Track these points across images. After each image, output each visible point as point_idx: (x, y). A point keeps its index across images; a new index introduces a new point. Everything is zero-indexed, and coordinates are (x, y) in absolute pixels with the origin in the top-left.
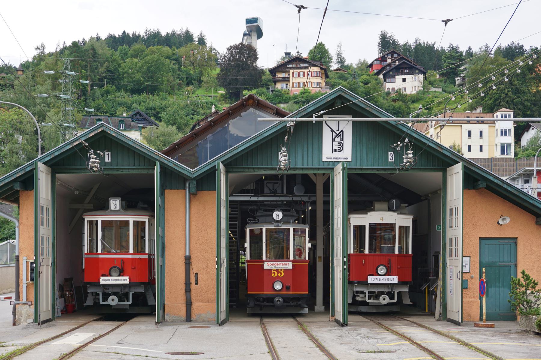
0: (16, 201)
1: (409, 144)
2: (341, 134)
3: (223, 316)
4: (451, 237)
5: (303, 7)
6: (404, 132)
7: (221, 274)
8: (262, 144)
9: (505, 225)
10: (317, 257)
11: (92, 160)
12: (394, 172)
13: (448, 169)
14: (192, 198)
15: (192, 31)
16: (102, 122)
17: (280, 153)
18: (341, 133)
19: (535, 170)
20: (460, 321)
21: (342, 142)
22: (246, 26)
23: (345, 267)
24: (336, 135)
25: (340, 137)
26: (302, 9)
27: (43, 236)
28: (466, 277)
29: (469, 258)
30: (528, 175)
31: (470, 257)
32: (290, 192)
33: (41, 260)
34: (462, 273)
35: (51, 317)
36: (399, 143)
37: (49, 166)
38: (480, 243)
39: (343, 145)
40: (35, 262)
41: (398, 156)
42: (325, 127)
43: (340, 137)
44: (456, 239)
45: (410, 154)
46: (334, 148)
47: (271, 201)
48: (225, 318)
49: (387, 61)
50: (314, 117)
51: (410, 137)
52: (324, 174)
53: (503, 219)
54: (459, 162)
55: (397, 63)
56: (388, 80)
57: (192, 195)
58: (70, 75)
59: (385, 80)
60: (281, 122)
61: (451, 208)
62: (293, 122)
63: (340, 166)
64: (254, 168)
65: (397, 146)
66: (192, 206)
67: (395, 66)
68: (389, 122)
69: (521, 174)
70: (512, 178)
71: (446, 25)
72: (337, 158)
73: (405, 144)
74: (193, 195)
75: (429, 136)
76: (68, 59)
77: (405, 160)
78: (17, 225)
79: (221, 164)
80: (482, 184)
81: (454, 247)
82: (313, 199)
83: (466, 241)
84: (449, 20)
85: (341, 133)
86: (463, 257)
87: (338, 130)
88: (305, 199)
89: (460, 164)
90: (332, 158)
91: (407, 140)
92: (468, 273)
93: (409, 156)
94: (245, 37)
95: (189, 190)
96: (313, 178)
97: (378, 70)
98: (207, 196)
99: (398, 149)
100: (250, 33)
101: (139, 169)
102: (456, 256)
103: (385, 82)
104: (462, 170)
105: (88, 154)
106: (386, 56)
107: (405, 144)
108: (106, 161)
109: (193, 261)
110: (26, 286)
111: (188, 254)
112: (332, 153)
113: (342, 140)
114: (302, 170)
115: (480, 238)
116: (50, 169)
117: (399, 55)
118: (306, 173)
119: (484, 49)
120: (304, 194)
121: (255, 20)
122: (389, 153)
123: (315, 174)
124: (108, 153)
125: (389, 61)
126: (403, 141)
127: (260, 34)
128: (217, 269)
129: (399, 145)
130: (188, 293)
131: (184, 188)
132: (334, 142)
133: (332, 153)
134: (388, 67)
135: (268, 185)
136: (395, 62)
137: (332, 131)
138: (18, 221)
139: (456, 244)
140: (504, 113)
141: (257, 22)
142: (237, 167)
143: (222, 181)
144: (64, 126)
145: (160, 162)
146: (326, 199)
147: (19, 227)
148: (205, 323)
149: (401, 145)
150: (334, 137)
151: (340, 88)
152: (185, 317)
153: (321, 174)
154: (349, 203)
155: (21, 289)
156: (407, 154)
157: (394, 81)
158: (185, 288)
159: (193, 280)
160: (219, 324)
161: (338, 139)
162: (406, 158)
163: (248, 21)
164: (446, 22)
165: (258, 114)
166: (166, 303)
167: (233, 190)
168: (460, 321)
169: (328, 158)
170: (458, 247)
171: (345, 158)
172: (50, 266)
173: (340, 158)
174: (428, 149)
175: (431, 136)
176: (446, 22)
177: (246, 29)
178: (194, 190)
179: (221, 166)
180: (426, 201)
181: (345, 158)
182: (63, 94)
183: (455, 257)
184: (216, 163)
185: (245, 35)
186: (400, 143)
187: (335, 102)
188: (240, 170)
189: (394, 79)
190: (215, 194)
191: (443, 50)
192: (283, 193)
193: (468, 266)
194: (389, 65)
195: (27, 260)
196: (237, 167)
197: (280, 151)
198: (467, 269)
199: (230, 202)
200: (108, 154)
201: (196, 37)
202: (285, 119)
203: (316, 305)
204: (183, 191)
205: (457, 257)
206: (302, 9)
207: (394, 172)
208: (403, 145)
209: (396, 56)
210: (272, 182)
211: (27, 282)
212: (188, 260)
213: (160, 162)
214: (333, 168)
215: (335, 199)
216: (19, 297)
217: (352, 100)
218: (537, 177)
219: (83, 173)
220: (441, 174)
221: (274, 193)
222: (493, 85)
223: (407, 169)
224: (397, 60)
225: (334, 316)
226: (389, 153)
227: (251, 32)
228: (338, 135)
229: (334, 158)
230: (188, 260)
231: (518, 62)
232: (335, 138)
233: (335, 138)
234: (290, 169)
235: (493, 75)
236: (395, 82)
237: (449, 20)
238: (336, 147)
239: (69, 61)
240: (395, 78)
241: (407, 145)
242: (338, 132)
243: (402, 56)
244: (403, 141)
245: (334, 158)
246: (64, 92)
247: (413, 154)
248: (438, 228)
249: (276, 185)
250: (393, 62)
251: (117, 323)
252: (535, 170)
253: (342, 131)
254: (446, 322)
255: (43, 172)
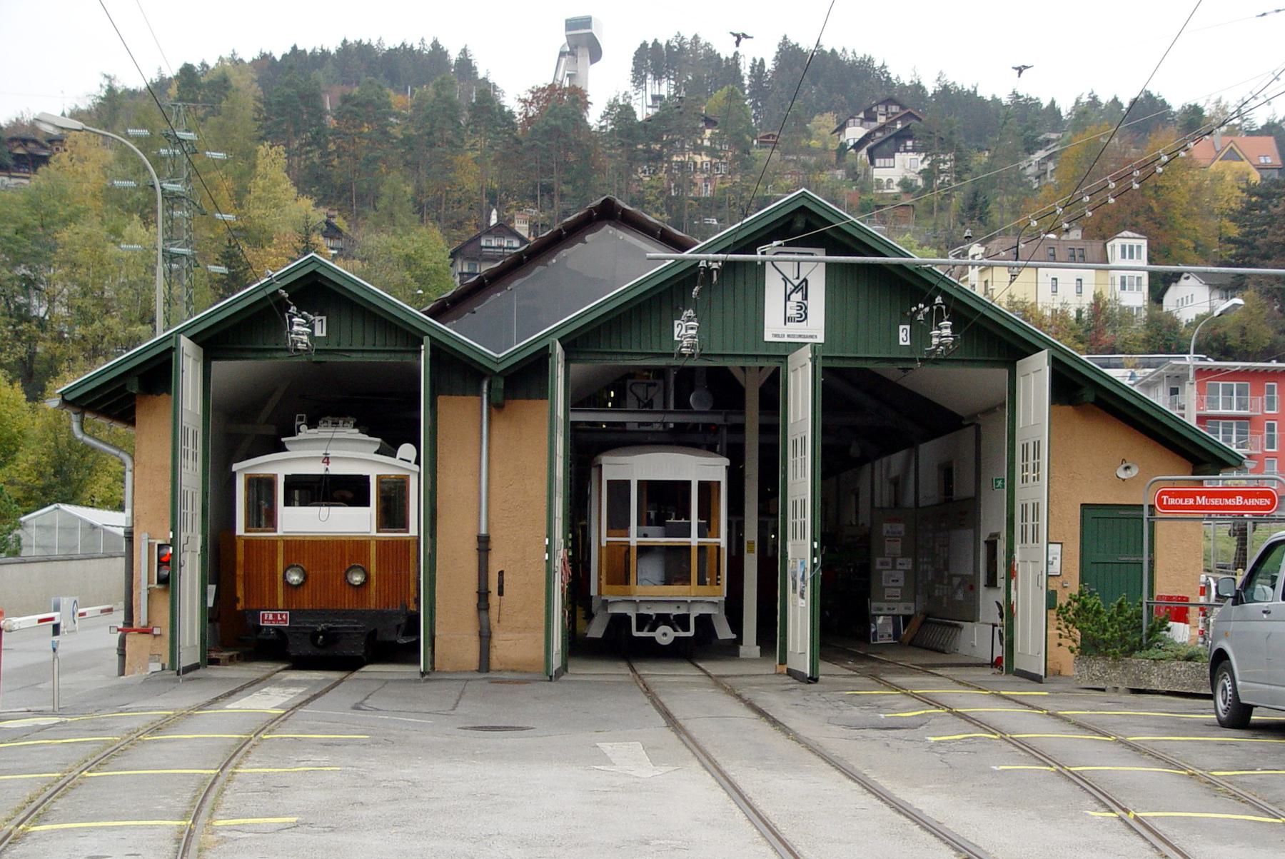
0: (128, 418)
1: (944, 307)
2: (803, 287)
3: (556, 662)
4: (1024, 503)
5: (744, 36)
6: (931, 285)
7: (555, 572)
8: (640, 304)
9: (1132, 479)
10: (746, 544)
11: (295, 328)
12: (910, 366)
13: (1019, 363)
14: (494, 418)
15: (445, 44)
16: (313, 254)
17: (676, 322)
18: (804, 284)
19: (1191, 367)
20: (1043, 673)
21: (805, 302)
22: (567, 36)
23: (815, 560)
24: (793, 288)
25: (800, 293)
26: (743, 40)
27: (187, 489)
28: (1054, 585)
29: (1060, 546)
30: (1177, 377)
31: (1061, 543)
32: (682, 405)
33: (183, 540)
34: (1048, 576)
35: (198, 660)
36: (921, 306)
37: (198, 344)
38: (1082, 516)
39: (806, 308)
40: (173, 542)
41: (920, 334)
42: (770, 272)
43: (800, 293)
44: (1036, 507)
45: (946, 328)
46: (788, 315)
47: (640, 424)
48: (560, 665)
49: (875, 120)
50: (759, 253)
51: (946, 295)
52: (761, 368)
53: (1127, 468)
54: (1041, 350)
55: (899, 126)
56: (878, 162)
57: (493, 409)
58: (184, 140)
59: (872, 163)
60: (679, 262)
61: (1025, 442)
62: (717, 262)
63: (806, 353)
64: (623, 354)
65: (918, 311)
66: (495, 432)
67: (895, 131)
68: (907, 266)
69: (1163, 374)
70: (1144, 384)
71: (1019, 76)
72: (793, 336)
73: (935, 307)
74: (496, 406)
75: (967, 287)
76: (180, 104)
77: (935, 341)
78: (129, 465)
79: (558, 343)
80: (1089, 396)
81: (1030, 523)
82: (735, 419)
83: (1054, 509)
84: (1026, 67)
85: (804, 284)
86: (1048, 543)
87: (798, 278)
88: (717, 419)
89: (1045, 352)
90: (784, 336)
91: (938, 300)
92: (1058, 576)
93: (944, 332)
94: (563, 60)
95: (489, 397)
96: (739, 375)
97: (856, 141)
98: (529, 412)
99: (919, 318)
100: (575, 50)
101: (384, 351)
102: (1036, 538)
103: (872, 167)
104: (1048, 364)
105: (287, 315)
106: (875, 109)
107: (935, 307)
108: (766, 339)
109: (494, 545)
110: (148, 595)
111: (483, 531)
112: (785, 324)
113: (805, 297)
114: (722, 359)
115: (1082, 505)
116: (201, 350)
117: (902, 108)
118: (721, 365)
119: (1085, 99)
120: (712, 408)
121: (586, 22)
122: (901, 327)
123: (743, 368)
124: (320, 318)
125: (882, 120)
126: (929, 302)
127: (595, 53)
128: (547, 561)
129: (922, 309)
130: (483, 614)
131: (478, 393)
132: (788, 303)
133: (785, 324)
134: (878, 134)
135: (634, 388)
136: (894, 122)
137: (785, 279)
138: (132, 458)
139: (1036, 516)
140: (1128, 242)
141: (590, 27)
142: (590, 350)
143: (559, 379)
144: (169, 251)
145: (431, 338)
146: (768, 420)
147: (133, 471)
148: (521, 676)
149: (927, 309)
150: (788, 292)
151: (804, 192)
152: (478, 664)
153: (756, 367)
154: (380, 541)
155: (137, 600)
156: (940, 329)
157: (892, 165)
158: (477, 602)
159: (493, 587)
160: (551, 677)
161: (797, 297)
162: (937, 337)
163: (571, 24)
164: (1020, 70)
165: (621, 238)
166: (437, 633)
167: (578, 400)
168: (1043, 673)
169: (776, 336)
170: (1040, 523)
171: (811, 337)
172: (199, 552)
173: (800, 336)
174: (985, 324)
175: (973, 286)
176: (1020, 70)
177: (564, 40)
178: (498, 397)
179: (558, 347)
180: (972, 428)
181: (811, 337)
182: (170, 182)
183: (1033, 542)
184: (549, 341)
185: (562, 54)
186: (923, 306)
187: (792, 220)
188: (593, 357)
189: (892, 160)
190: (543, 405)
191: (996, 101)
192: (665, 404)
193: (1057, 563)
194: (882, 128)
195: (150, 541)
196: (590, 350)
197: (679, 319)
198: (1055, 569)
199: (574, 424)
200: (322, 320)
201: (454, 56)
202: (686, 254)
203: (742, 644)
204: (475, 399)
205: (1037, 542)
206: (743, 40)
207: (910, 366)
208: (931, 309)
209: (894, 109)
210: (643, 383)
211: (150, 586)
212: (484, 544)
213: (431, 338)
214: (786, 357)
215: (791, 420)
216: (132, 616)
217: (833, 221)
218: (1196, 382)
219: (270, 358)
220: (1004, 373)
221: (647, 406)
222: (1109, 195)
223: (937, 361)
224: (898, 119)
225: (786, 663)
226: (901, 327)
227: (576, 47)
228: (796, 289)
229: (789, 336)
230: (484, 544)
231: (1159, 154)
232: (791, 293)
233: (791, 293)
234: (702, 356)
235: (1111, 178)
236: (894, 167)
237: (1026, 67)
238: (792, 312)
239: (182, 109)
240: (893, 157)
241: (939, 309)
242: (796, 283)
243: (910, 110)
244: (929, 302)
245: (789, 336)
246: (172, 177)
247: (952, 328)
248: (996, 484)
249: (652, 390)
250: (889, 124)
251: (334, 676)
252: (1191, 367)
253: (805, 280)
254: (1011, 678)
255: (189, 356)
